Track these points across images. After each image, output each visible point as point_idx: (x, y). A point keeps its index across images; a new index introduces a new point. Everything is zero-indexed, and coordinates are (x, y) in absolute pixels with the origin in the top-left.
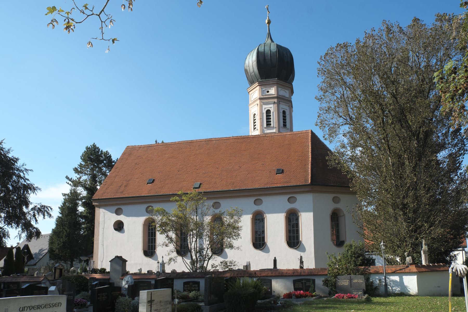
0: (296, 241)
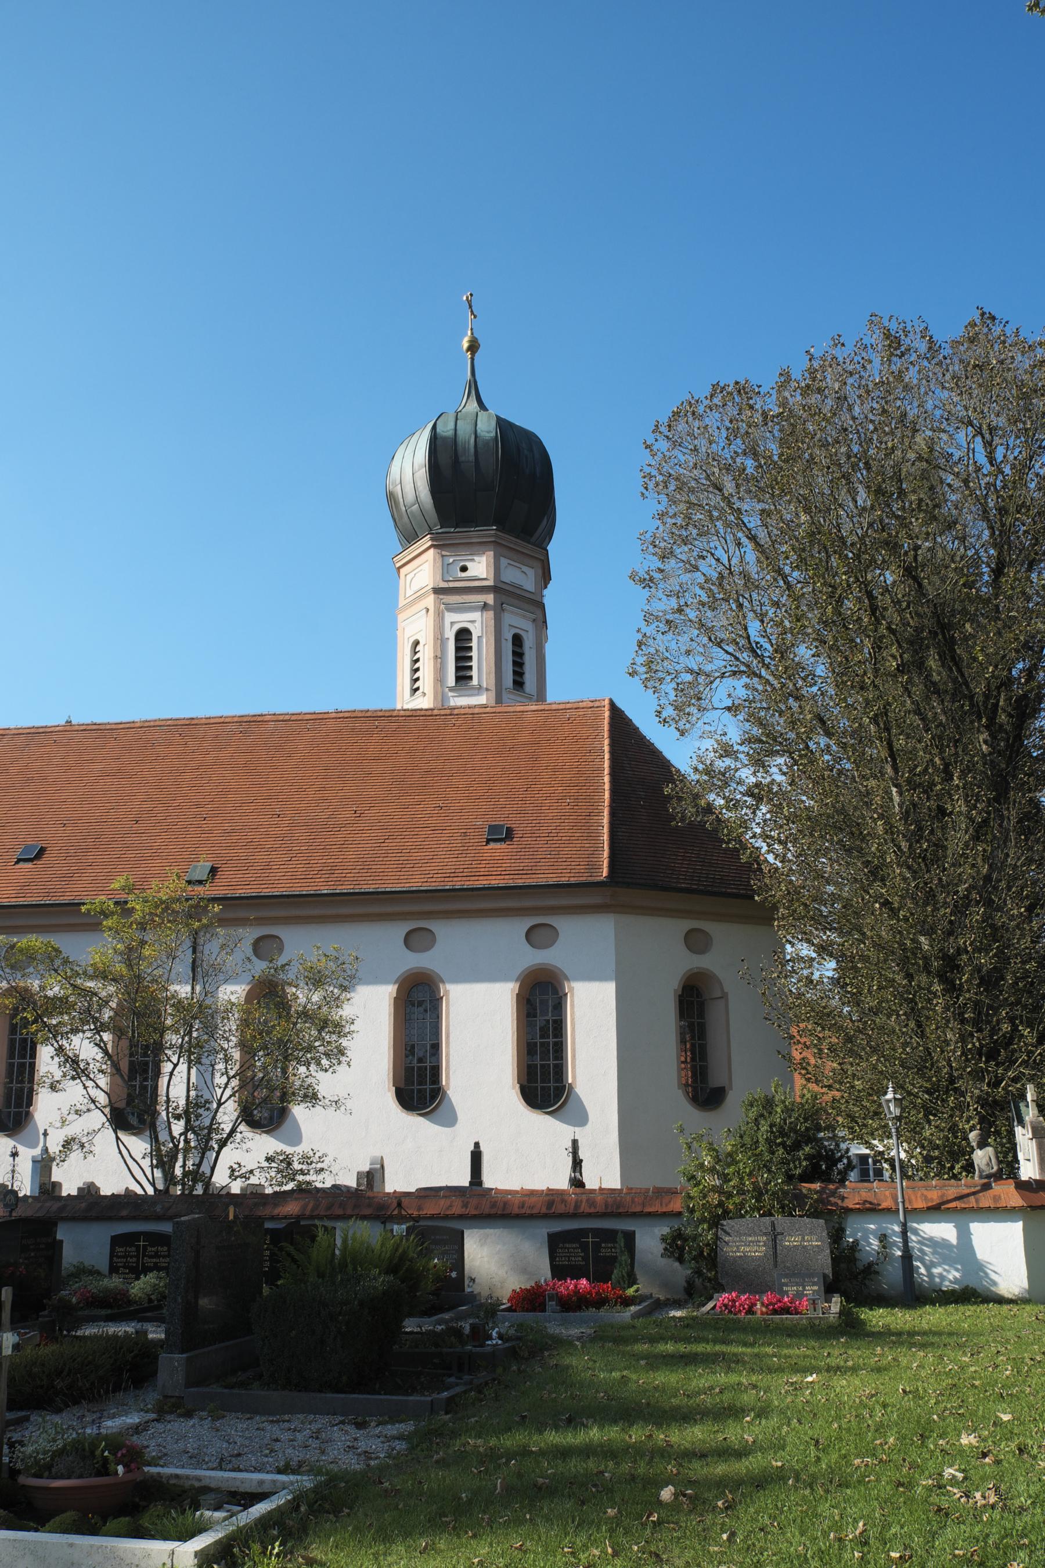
0: (552, 1084)
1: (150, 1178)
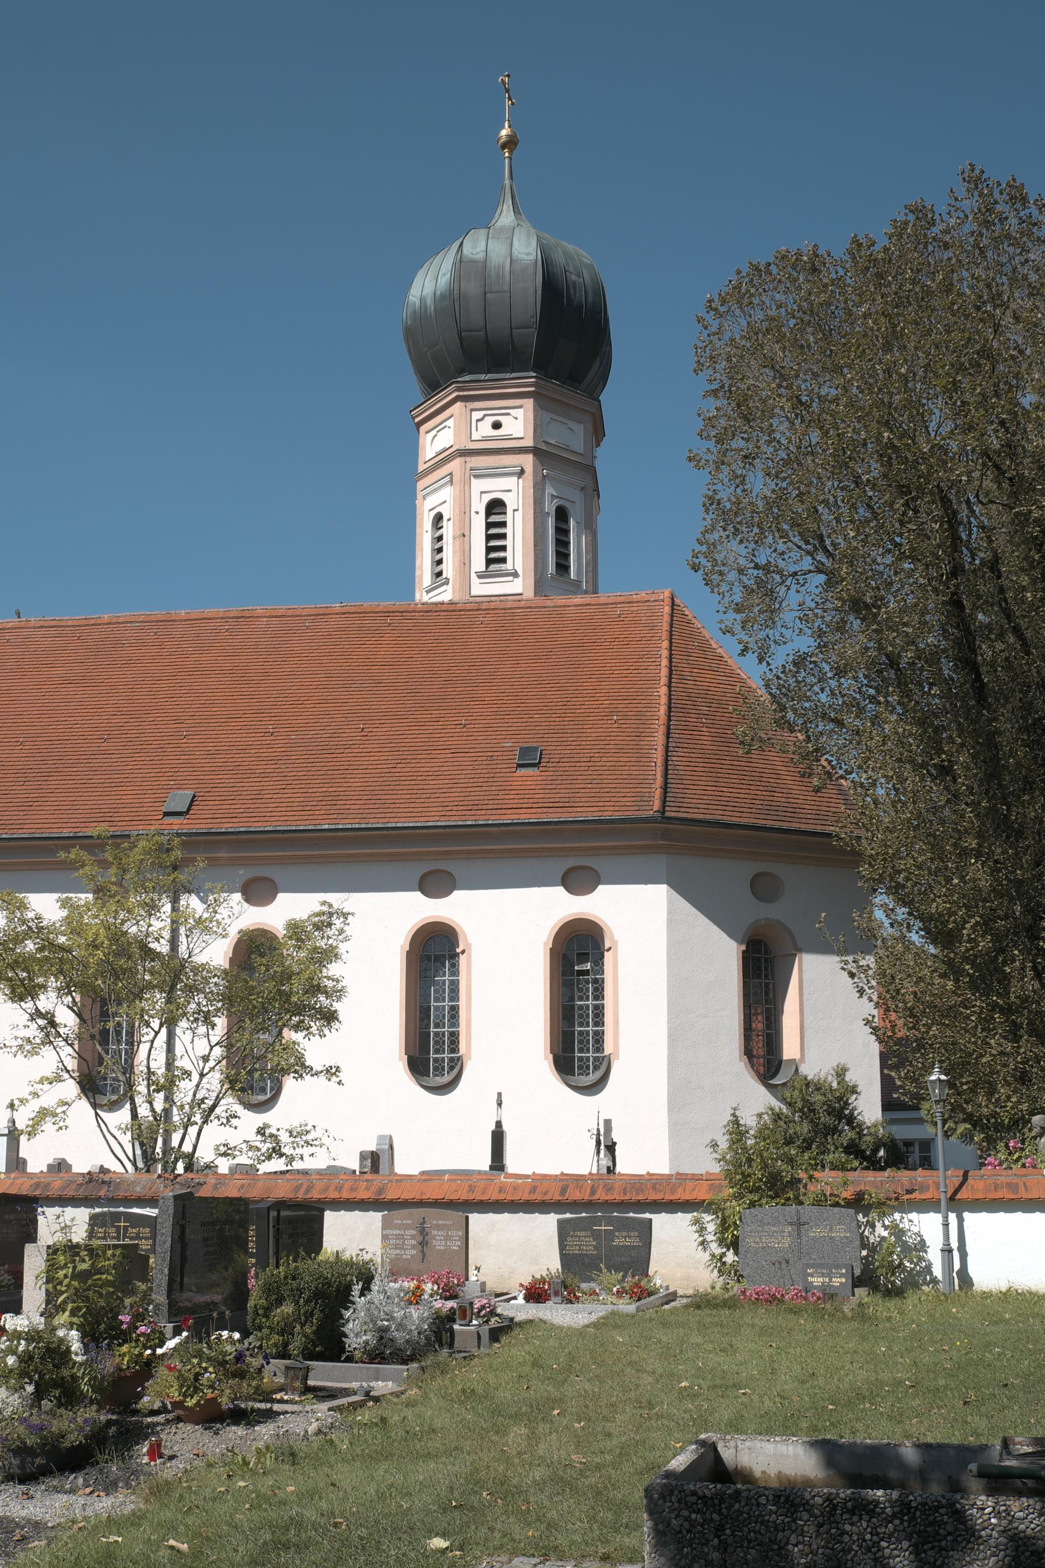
1: (131, 1158)
